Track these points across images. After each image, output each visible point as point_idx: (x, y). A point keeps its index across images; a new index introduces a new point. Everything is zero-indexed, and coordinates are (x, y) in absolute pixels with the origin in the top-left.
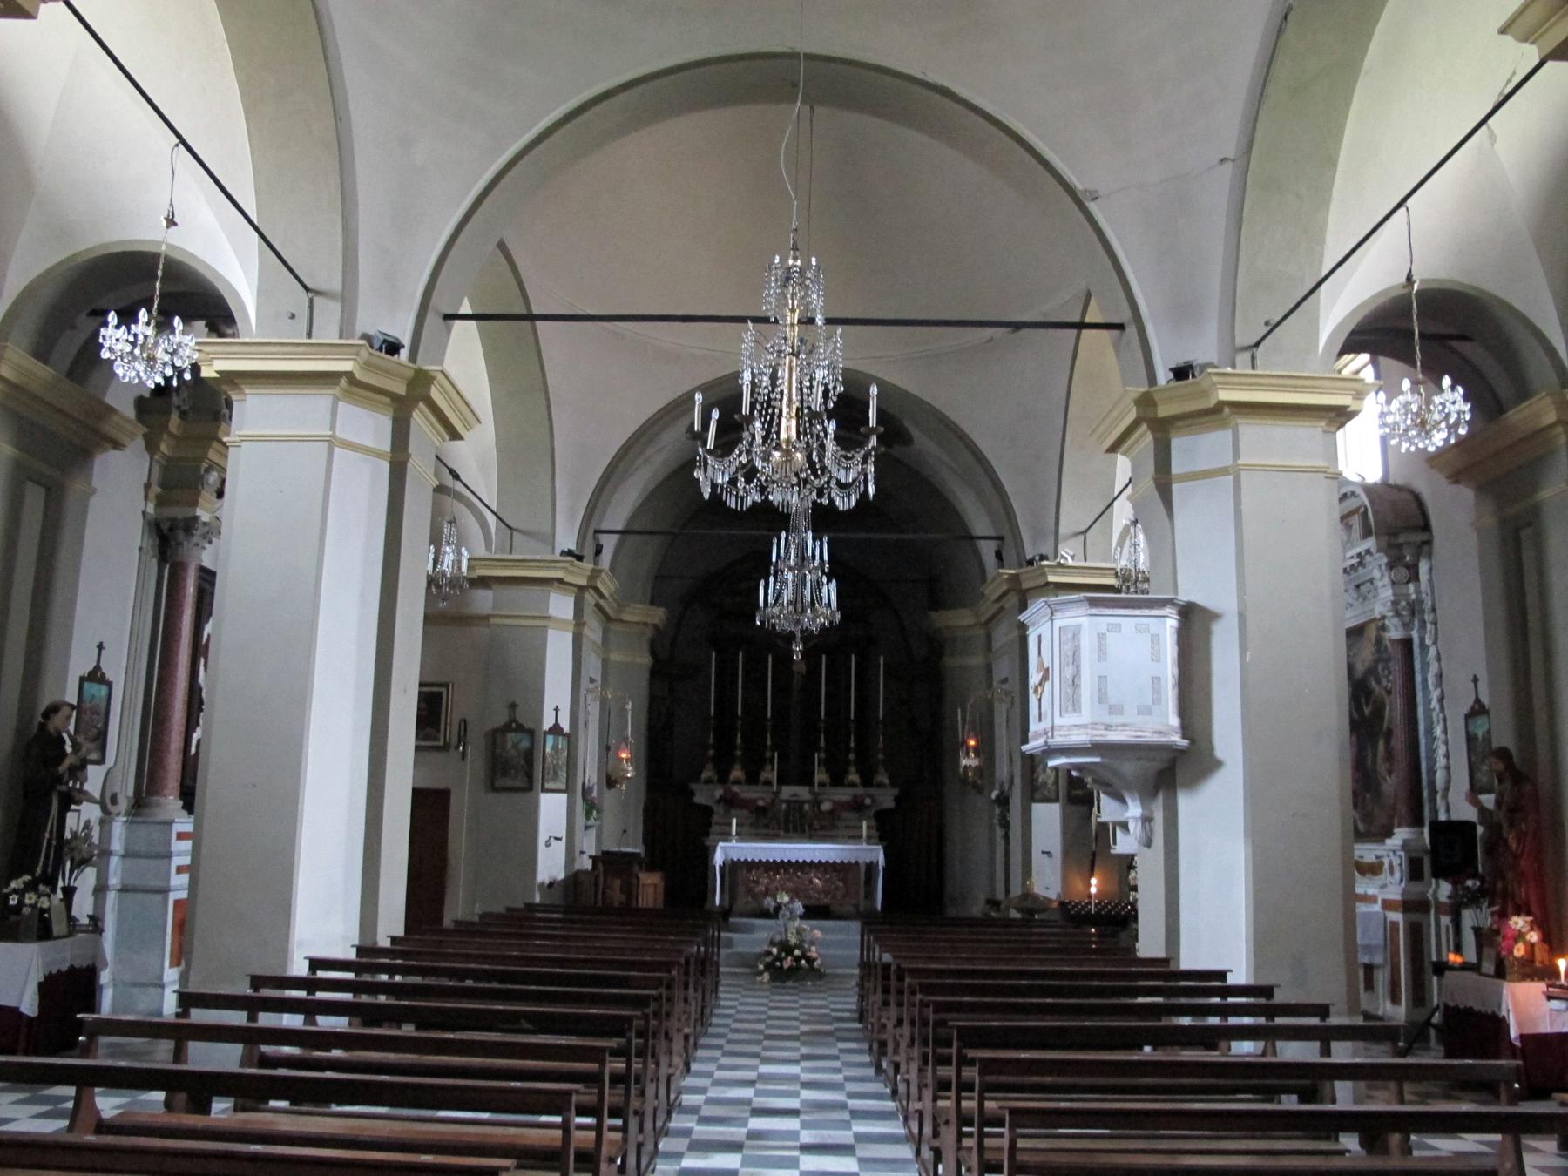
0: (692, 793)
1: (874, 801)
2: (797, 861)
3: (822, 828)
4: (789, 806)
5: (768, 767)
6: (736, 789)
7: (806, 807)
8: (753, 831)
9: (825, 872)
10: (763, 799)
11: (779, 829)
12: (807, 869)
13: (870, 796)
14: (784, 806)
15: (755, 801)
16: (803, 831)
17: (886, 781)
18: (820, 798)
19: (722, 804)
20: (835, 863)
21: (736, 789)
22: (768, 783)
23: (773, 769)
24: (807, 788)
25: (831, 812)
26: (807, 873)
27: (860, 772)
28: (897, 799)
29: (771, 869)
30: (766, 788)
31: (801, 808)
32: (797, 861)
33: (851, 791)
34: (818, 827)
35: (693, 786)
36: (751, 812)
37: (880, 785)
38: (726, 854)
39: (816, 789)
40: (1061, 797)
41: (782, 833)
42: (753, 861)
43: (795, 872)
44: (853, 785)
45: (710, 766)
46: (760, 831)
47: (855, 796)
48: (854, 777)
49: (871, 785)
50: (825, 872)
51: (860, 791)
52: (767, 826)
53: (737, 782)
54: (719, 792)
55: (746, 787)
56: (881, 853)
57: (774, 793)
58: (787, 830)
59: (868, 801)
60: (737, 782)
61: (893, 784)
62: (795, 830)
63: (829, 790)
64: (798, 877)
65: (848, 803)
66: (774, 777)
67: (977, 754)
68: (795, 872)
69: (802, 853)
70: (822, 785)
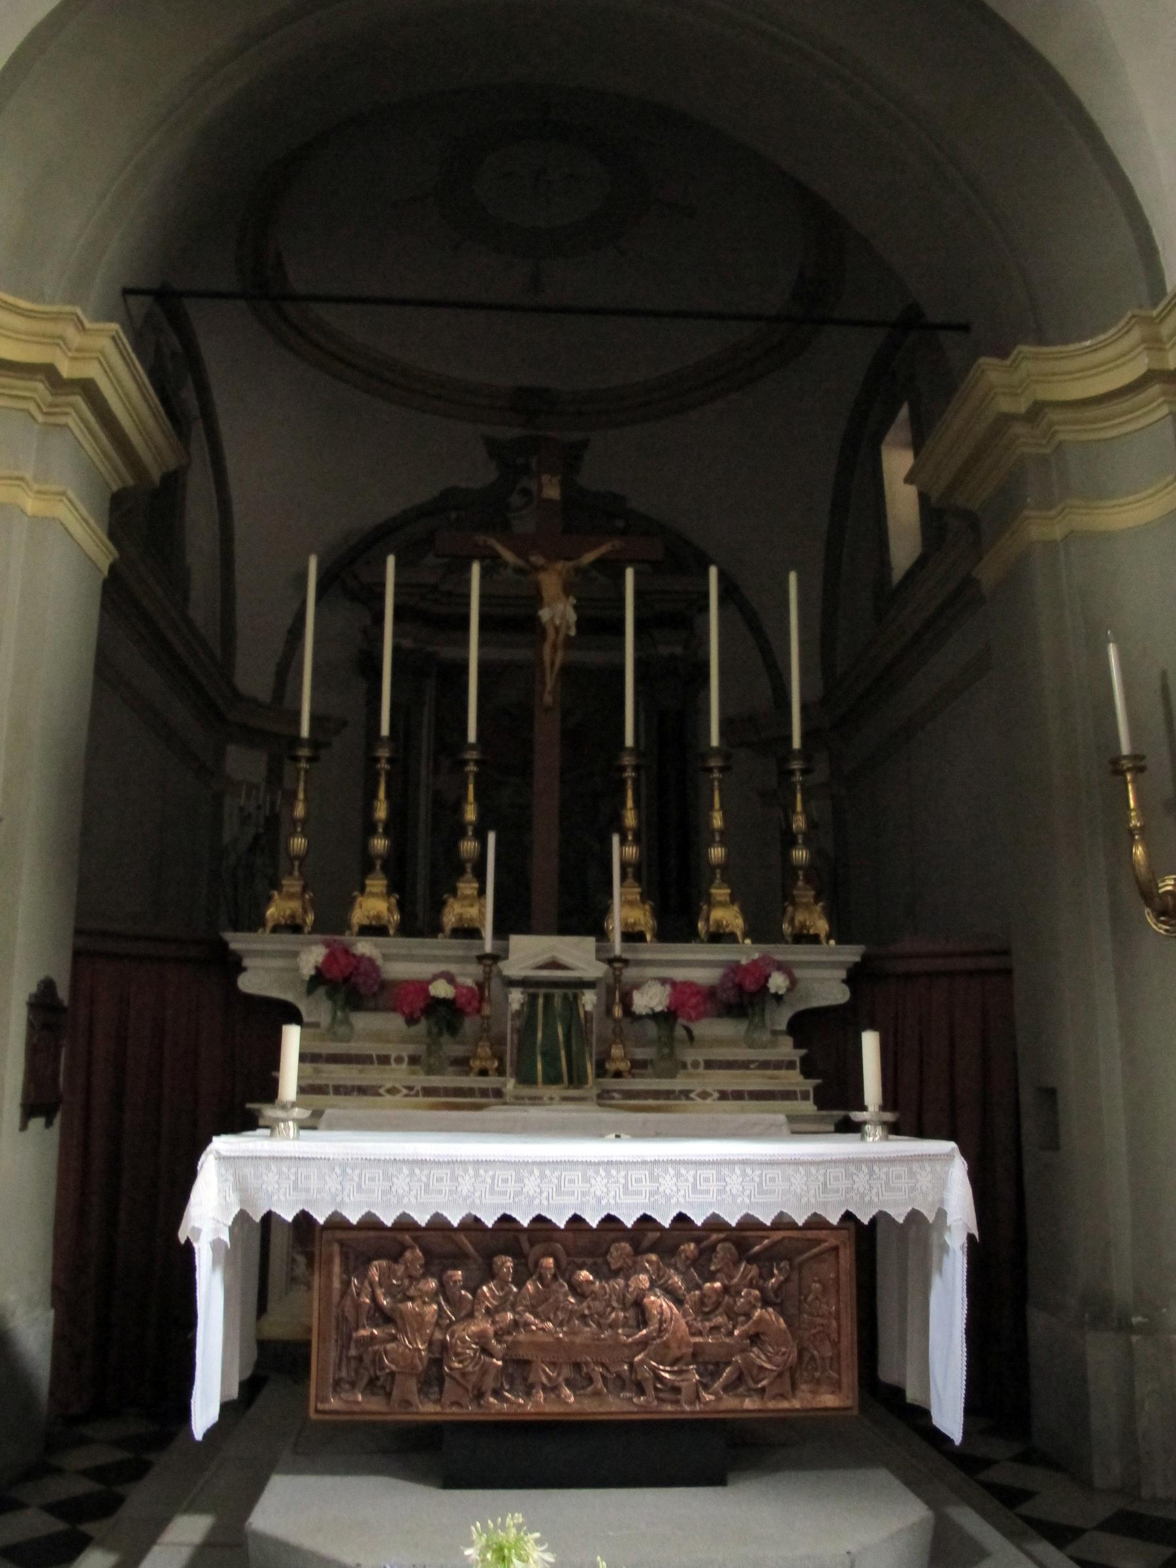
0: (233, 965)
1: (793, 982)
2: (576, 1220)
3: (638, 1066)
4: (532, 1000)
5: (467, 887)
6: (365, 947)
7: (589, 1000)
8: (422, 1080)
9: (701, 1265)
10: (450, 978)
11: (501, 1072)
12: (621, 1250)
13: (782, 967)
14: (516, 997)
15: (421, 986)
16: (577, 1079)
17: (821, 926)
18: (630, 974)
19: (321, 991)
20: (749, 1224)
21: (365, 947)
22: (470, 932)
23: (482, 892)
24: (590, 942)
25: (665, 1018)
26: (626, 1272)
27: (399, 886)
28: (855, 977)
29: (458, 1258)
30: (458, 947)
31: (572, 1004)
32: (576, 1220)
33: (723, 953)
34: (624, 1066)
35: (237, 942)
36: (411, 1021)
37: (804, 937)
38: (242, 1188)
39: (617, 946)
40: (291, 948)
41: (510, 1084)
42: (370, 1224)
43: (564, 1271)
44: (718, 936)
45: (377, 883)
46: (436, 1081)
47: (734, 968)
48: (728, 916)
49: (434, 929)
50: (701, 1265)
51: (747, 952)
52: (462, 1064)
53: (375, 930)
54: (312, 957)
55: (396, 944)
56: (959, 1170)
57: (481, 958)
58: (526, 1078)
59: (777, 982)
60: (375, 930)
61: (842, 933)
62: (553, 1079)
63: (651, 950)
64: (576, 1289)
65: (710, 993)
66: (486, 913)
67: (637, 840)
68: (564, 1271)
69: (599, 1184)
70: (632, 936)
